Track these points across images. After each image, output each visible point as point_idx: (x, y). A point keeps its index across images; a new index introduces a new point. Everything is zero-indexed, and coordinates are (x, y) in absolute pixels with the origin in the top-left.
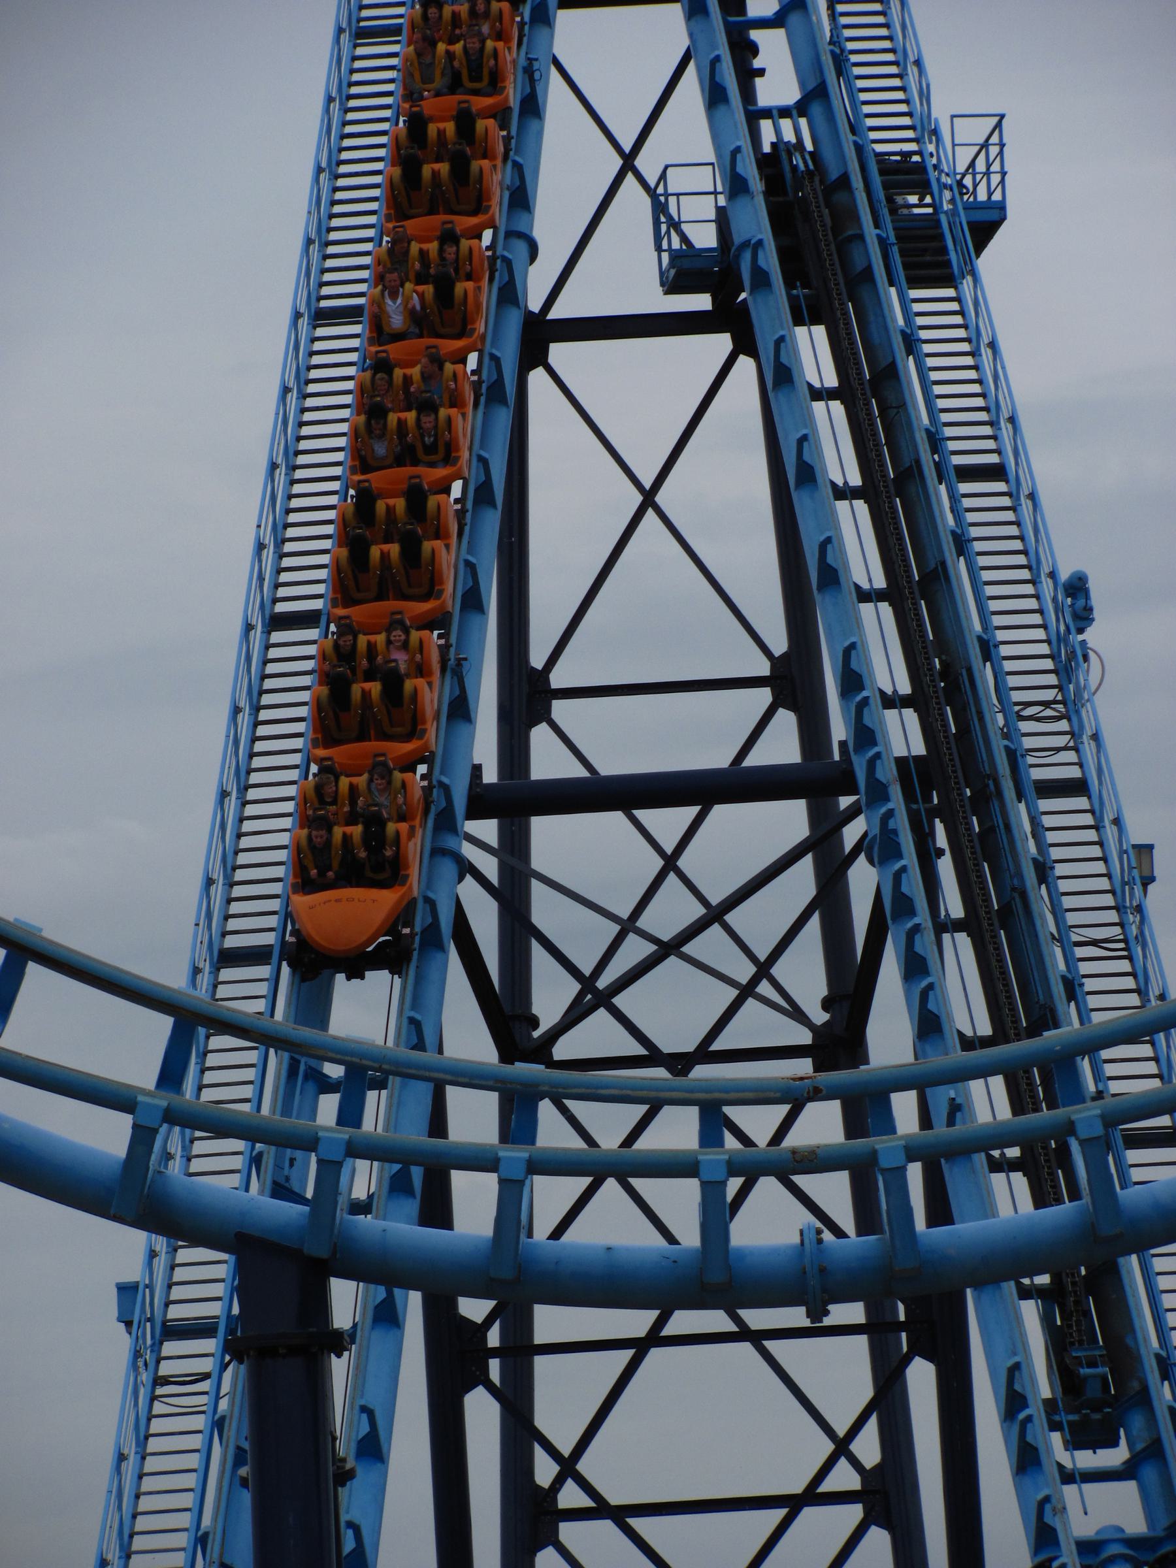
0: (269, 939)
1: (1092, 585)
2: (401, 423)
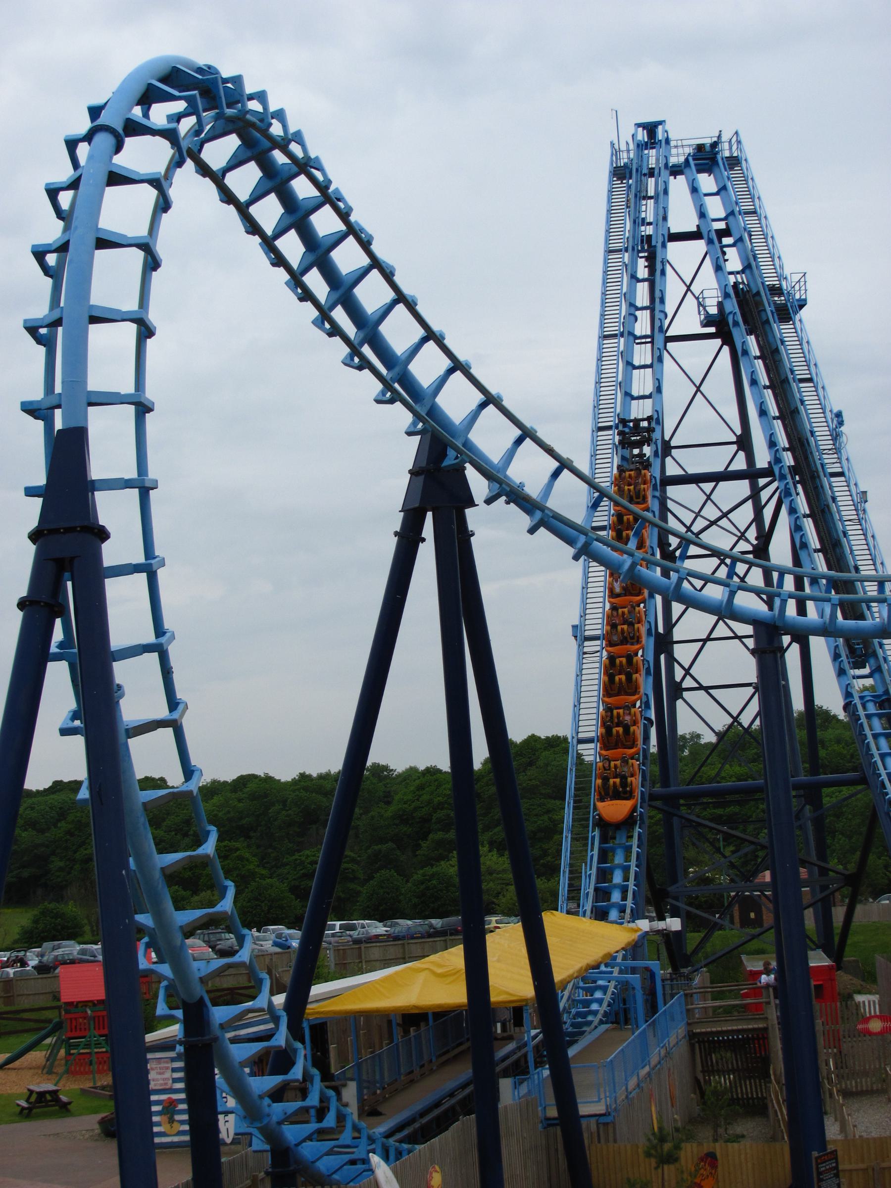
0: (605, 523)
1: (844, 414)
2: (622, 629)
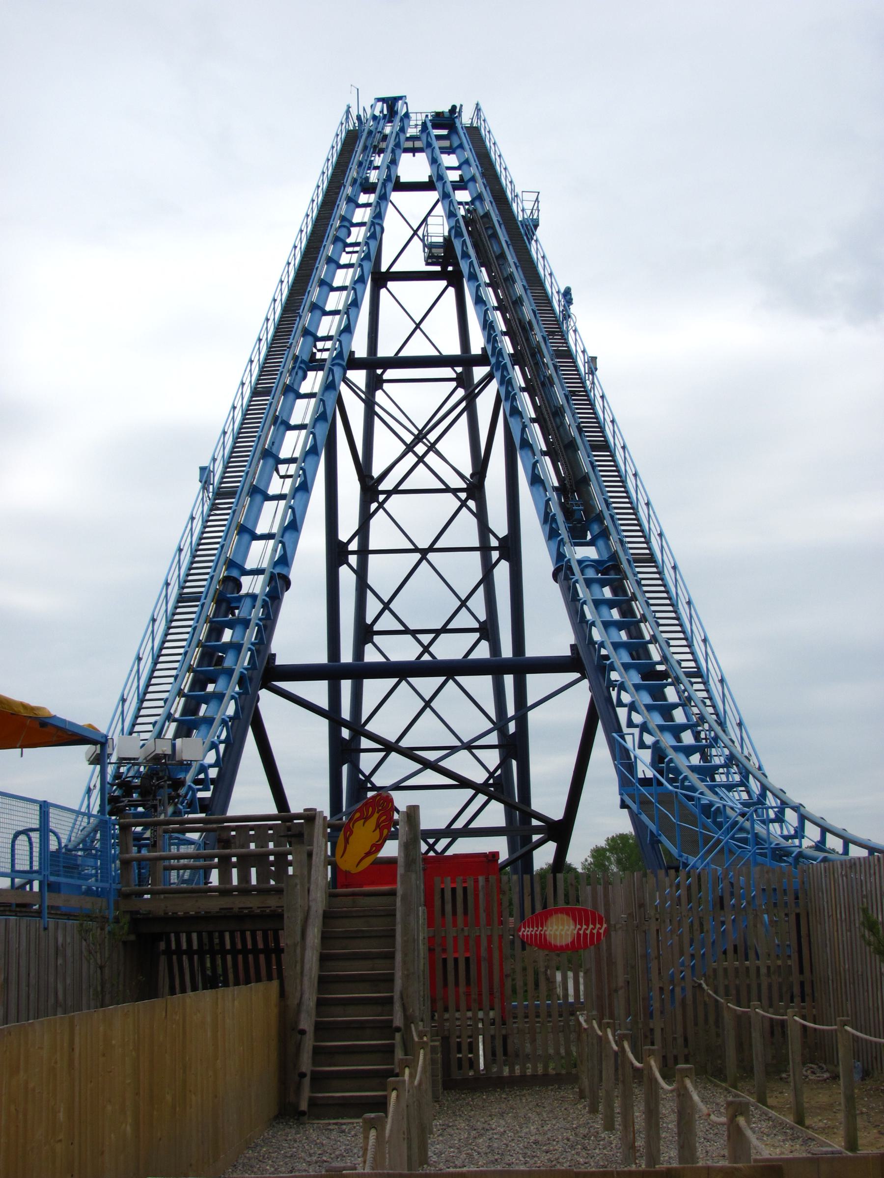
1: (572, 292)
